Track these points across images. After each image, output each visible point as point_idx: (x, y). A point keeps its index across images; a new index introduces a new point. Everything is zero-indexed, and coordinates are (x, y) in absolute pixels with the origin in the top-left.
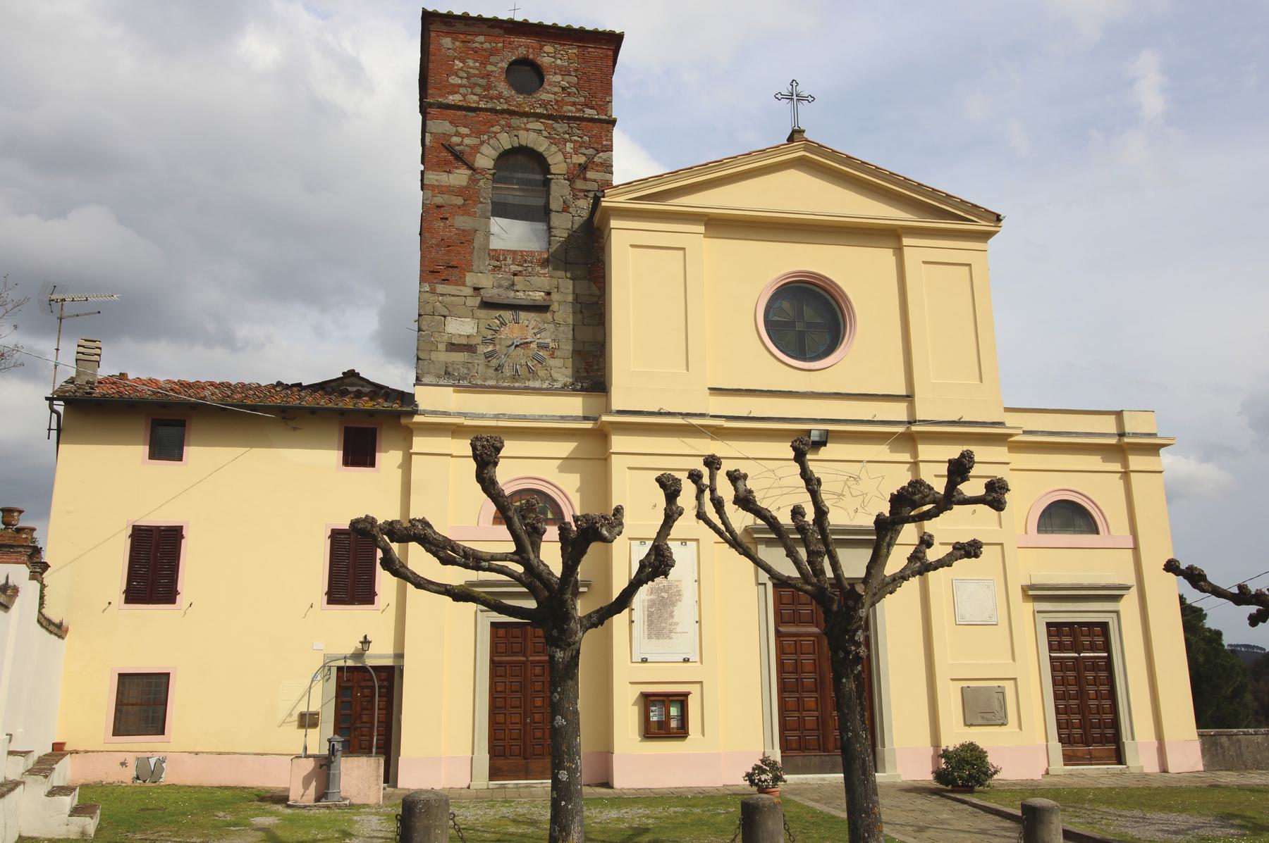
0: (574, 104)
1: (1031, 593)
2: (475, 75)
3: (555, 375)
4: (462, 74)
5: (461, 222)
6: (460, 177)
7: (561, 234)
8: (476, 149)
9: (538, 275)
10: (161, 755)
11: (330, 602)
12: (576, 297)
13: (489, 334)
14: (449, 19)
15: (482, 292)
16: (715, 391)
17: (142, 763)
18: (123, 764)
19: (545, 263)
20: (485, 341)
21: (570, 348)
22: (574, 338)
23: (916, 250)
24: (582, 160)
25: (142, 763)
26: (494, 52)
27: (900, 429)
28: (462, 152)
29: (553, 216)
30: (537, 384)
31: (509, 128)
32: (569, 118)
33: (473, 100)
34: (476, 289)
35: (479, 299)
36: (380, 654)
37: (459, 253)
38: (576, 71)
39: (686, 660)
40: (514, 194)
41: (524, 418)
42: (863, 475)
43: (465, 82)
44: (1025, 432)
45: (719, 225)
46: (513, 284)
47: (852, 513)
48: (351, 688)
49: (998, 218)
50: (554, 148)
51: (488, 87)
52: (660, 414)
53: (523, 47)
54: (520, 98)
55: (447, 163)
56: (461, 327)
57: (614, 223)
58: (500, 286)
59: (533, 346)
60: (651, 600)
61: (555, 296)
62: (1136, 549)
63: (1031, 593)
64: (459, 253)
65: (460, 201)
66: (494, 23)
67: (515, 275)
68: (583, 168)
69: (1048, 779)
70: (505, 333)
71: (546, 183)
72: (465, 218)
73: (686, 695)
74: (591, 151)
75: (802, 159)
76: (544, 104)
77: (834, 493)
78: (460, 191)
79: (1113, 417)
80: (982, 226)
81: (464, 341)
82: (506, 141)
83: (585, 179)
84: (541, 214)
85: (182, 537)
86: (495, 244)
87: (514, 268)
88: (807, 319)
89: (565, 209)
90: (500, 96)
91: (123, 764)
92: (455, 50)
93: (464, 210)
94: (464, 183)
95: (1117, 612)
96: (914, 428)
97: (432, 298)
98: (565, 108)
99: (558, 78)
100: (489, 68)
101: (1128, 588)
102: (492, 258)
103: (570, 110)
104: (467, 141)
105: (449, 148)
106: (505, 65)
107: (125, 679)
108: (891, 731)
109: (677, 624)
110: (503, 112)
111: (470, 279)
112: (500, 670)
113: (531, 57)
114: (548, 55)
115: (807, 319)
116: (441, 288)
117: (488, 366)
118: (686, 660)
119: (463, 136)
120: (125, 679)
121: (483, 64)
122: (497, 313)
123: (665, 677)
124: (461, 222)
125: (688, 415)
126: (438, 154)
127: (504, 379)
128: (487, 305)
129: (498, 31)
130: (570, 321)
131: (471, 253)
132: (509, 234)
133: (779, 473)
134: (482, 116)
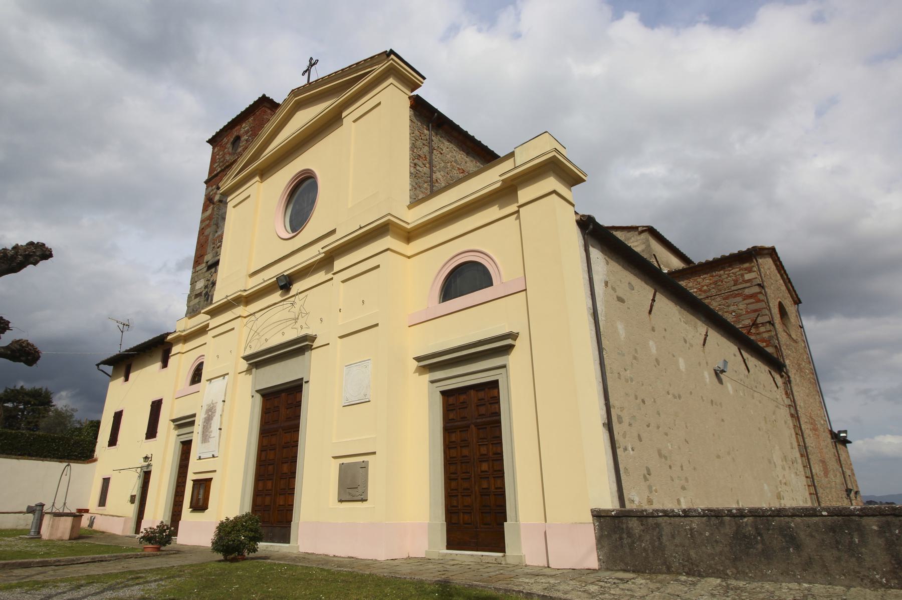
118: (213, 456)
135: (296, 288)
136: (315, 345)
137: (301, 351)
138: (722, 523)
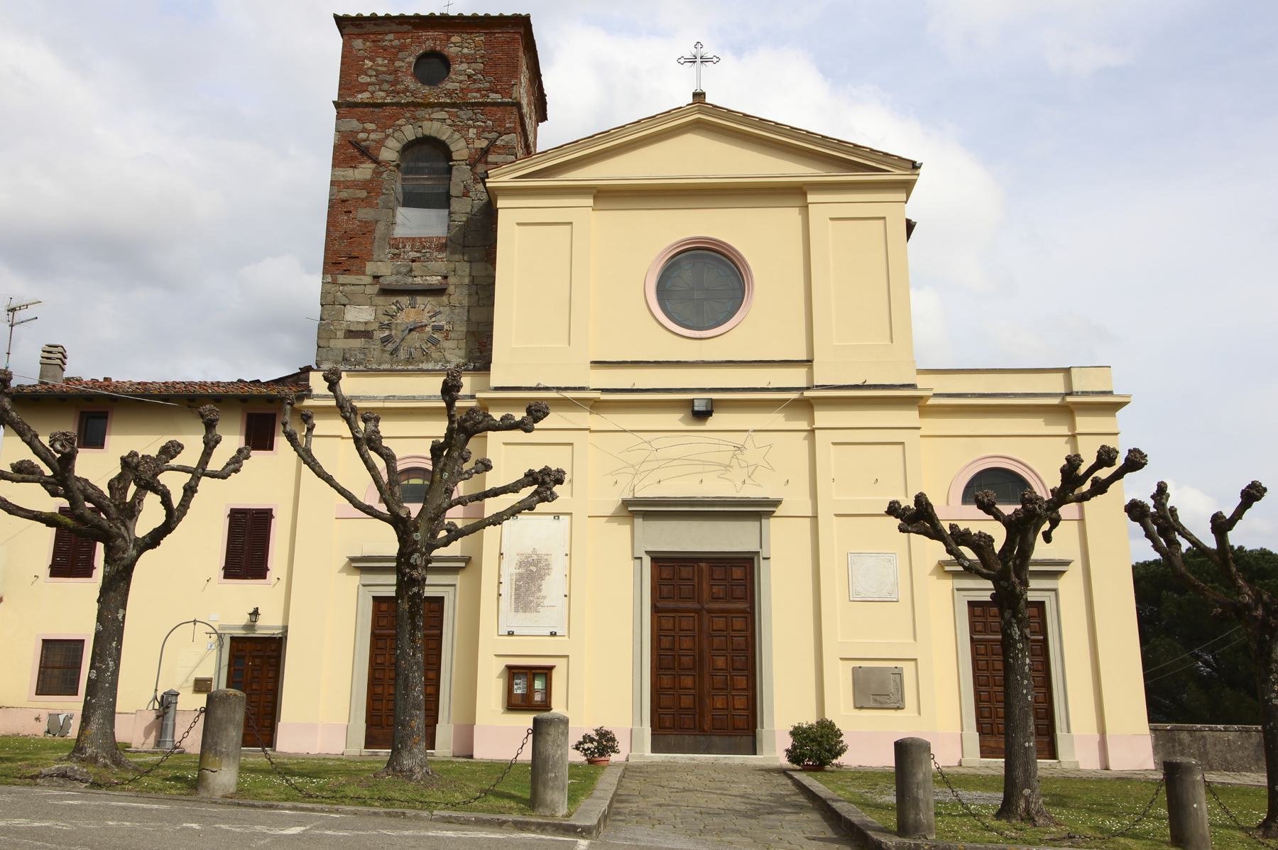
0: (478, 90)
1: (947, 568)
2: (384, 73)
3: (448, 357)
4: (370, 72)
5: (364, 214)
6: (364, 171)
7: (461, 218)
8: (381, 143)
9: (436, 260)
10: (70, 712)
11: (226, 577)
12: (473, 278)
13: (386, 320)
14: (359, 20)
15: (381, 280)
16: (597, 364)
17: (53, 717)
18: (37, 719)
19: (442, 247)
20: (382, 327)
21: (464, 329)
22: (469, 319)
23: (822, 207)
24: (484, 144)
25: (53, 717)
26: (402, 48)
27: (1056, 401)
28: (367, 148)
29: (453, 201)
30: (430, 366)
31: (415, 120)
32: (473, 104)
33: (380, 96)
34: (376, 277)
35: (377, 287)
36: (269, 624)
37: (360, 244)
38: (482, 57)
39: (553, 634)
40: (425, 182)
41: (414, 398)
42: (749, 445)
43: (373, 79)
44: (936, 395)
45: (606, 195)
46: (411, 271)
47: (739, 484)
48: (243, 657)
49: (915, 166)
50: (457, 135)
51: (395, 83)
52: (538, 389)
53: (430, 40)
54: (426, 90)
55: (353, 158)
56: (359, 315)
57: (501, 203)
58: (398, 273)
59: (429, 329)
60: (520, 574)
61: (451, 280)
62: (815, 517)
63: (947, 568)
64: (360, 244)
65: (363, 194)
66: (402, 19)
67: (413, 261)
68: (485, 152)
69: (961, 770)
70: (401, 318)
71: (449, 170)
72: (368, 209)
73: (551, 668)
74: (494, 135)
75: (698, 121)
76: (449, 94)
77: (720, 465)
78: (364, 185)
79: (1060, 376)
80: (897, 175)
81: (362, 328)
82: (410, 133)
83: (486, 163)
84: (443, 201)
85: (272, 517)
86: (399, 232)
87: (413, 255)
88: (703, 284)
89: (466, 194)
90: (407, 90)
91: (37, 719)
92: (365, 50)
93: (367, 202)
94: (368, 177)
95: (1055, 590)
96: (1069, 399)
97: (333, 288)
98: (470, 95)
99: (464, 66)
100: (398, 64)
101: (1067, 563)
102: (392, 246)
103: (474, 97)
104: (373, 136)
105: (356, 145)
106: (412, 59)
107: (47, 644)
108: (772, 712)
109: (544, 597)
110: (408, 104)
111: (370, 268)
112: (381, 644)
113: (438, 48)
114: (455, 46)
115: (703, 284)
116: (342, 279)
117: (383, 351)
118: (553, 634)
119: (369, 132)
120: (47, 644)
121: (392, 61)
122: (394, 299)
123: (530, 650)
124: (364, 214)
125: (559, 389)
126: (349, 150)
127: (398, 362)
128: (386, 292)
129: (406, 28)
130: (465, 303)
131: (372, 243)
132: (416, 223)
133: (655, 444)
134: (389, 111)
135: (718, 420)
136: (779, 511)
137: (758, 516)
138: (1250, 736)
